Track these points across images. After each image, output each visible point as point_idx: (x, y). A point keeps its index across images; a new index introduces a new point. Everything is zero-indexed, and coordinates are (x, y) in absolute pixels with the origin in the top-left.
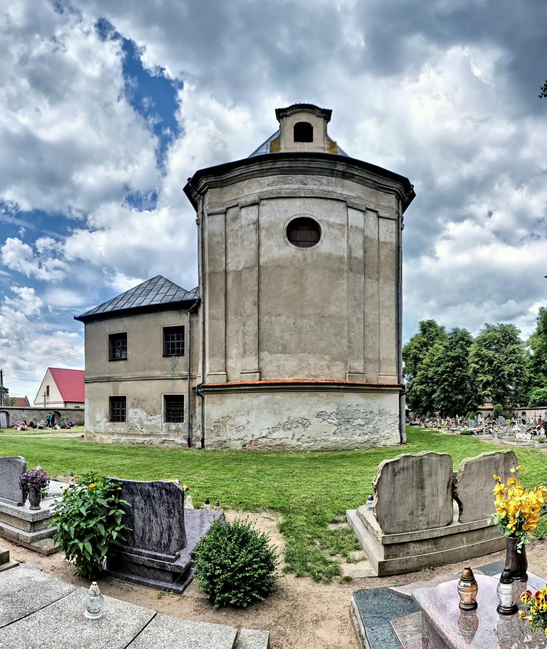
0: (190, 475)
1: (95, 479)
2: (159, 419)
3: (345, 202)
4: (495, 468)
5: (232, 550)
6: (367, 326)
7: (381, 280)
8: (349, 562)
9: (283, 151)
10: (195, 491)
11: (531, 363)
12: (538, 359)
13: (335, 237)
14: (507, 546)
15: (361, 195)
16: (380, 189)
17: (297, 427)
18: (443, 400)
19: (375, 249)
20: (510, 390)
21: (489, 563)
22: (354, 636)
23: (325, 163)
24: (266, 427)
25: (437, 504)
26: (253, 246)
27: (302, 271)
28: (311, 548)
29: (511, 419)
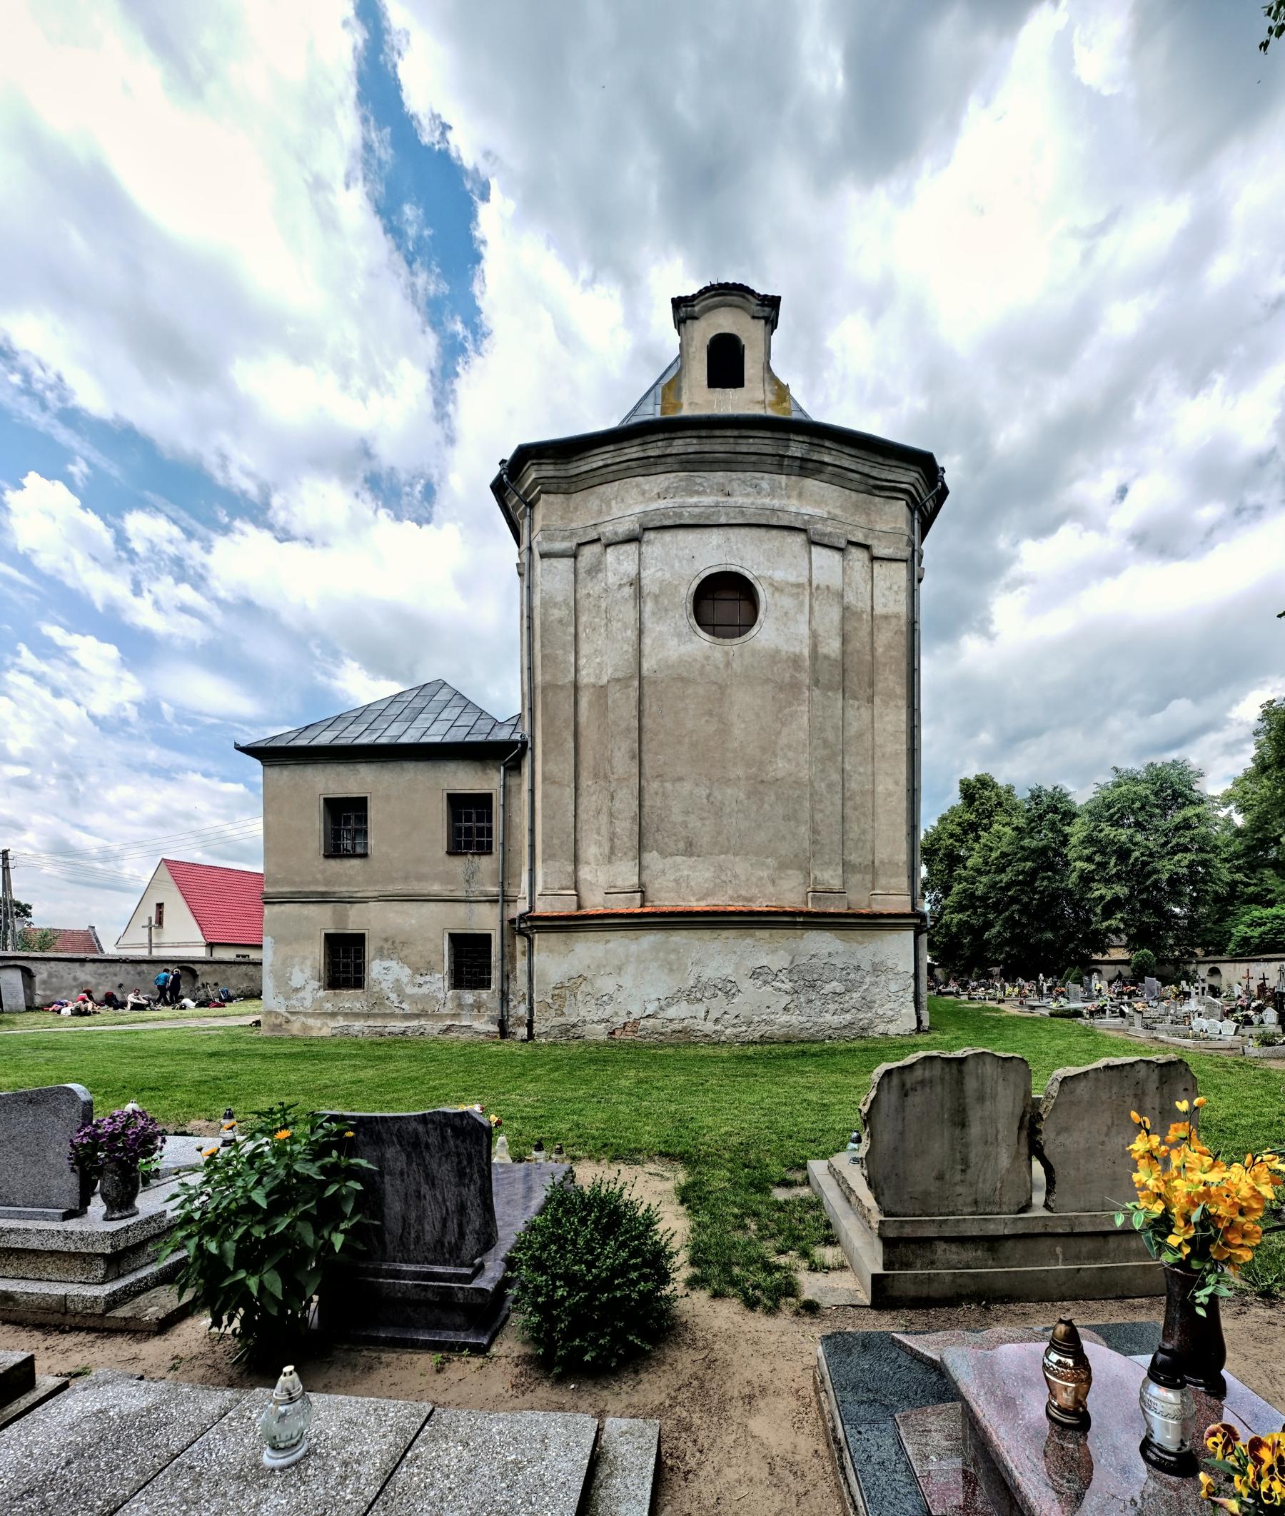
0: (504, 1094)
1: (289, 1119)
2: (439, 982)
3: (804, 531)
4: (1136, 1096)
5: (587, 1242)
6: (850, 799)
7: (877, 700)
8: (813, 1268)
9: (686, 411)
10: (515, 1125)
11: (1238, 845)
12: (1259, 835)
13: (786, 613)
14: (1169, 1289)
15: (838, 512)
16: (877, 492)
17: (715, 996)
18: (1007, 942)
19: (866, 628)
20: (1176, 916)
21: (1120, 1320)
22: (823, 1440)
23: (767, 441)
24: (653, 997)
25: (996, 1163)
26: (629, 632)
27: (722, 688)
28: (738, 1236)
29: (1177, 984)
